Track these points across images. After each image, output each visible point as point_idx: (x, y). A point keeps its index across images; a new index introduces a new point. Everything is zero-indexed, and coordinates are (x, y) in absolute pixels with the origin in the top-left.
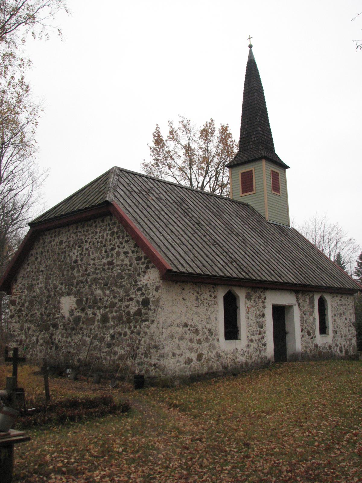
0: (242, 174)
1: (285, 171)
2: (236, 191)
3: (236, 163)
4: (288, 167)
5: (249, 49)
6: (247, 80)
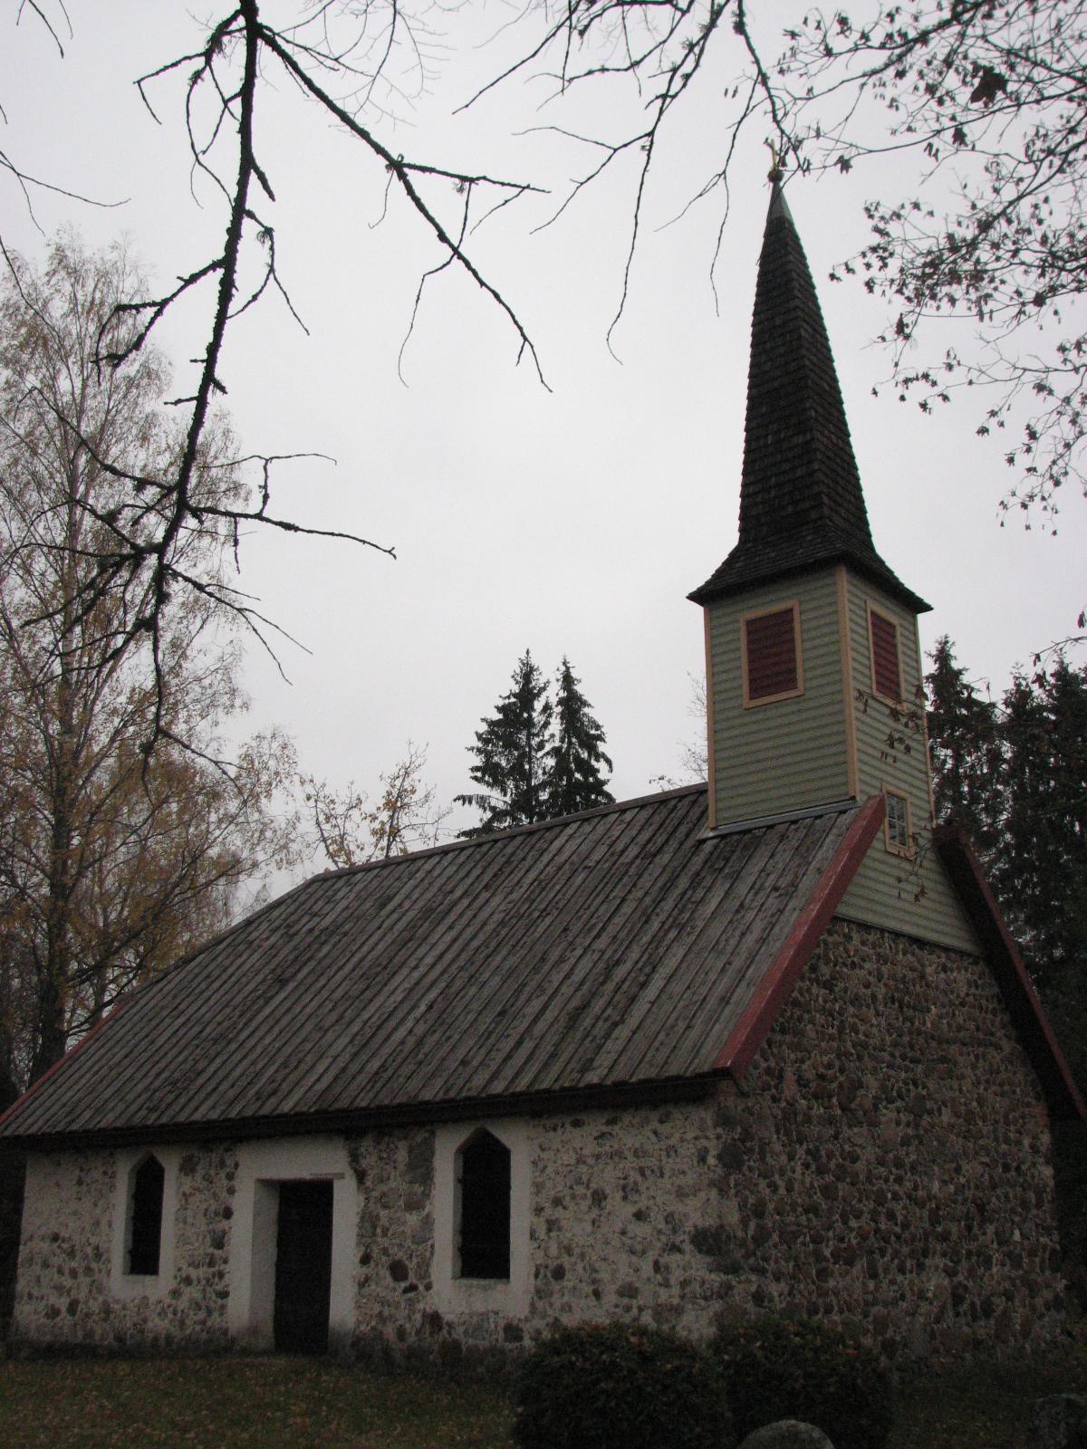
0: (750, 623)
1: (915, 619)
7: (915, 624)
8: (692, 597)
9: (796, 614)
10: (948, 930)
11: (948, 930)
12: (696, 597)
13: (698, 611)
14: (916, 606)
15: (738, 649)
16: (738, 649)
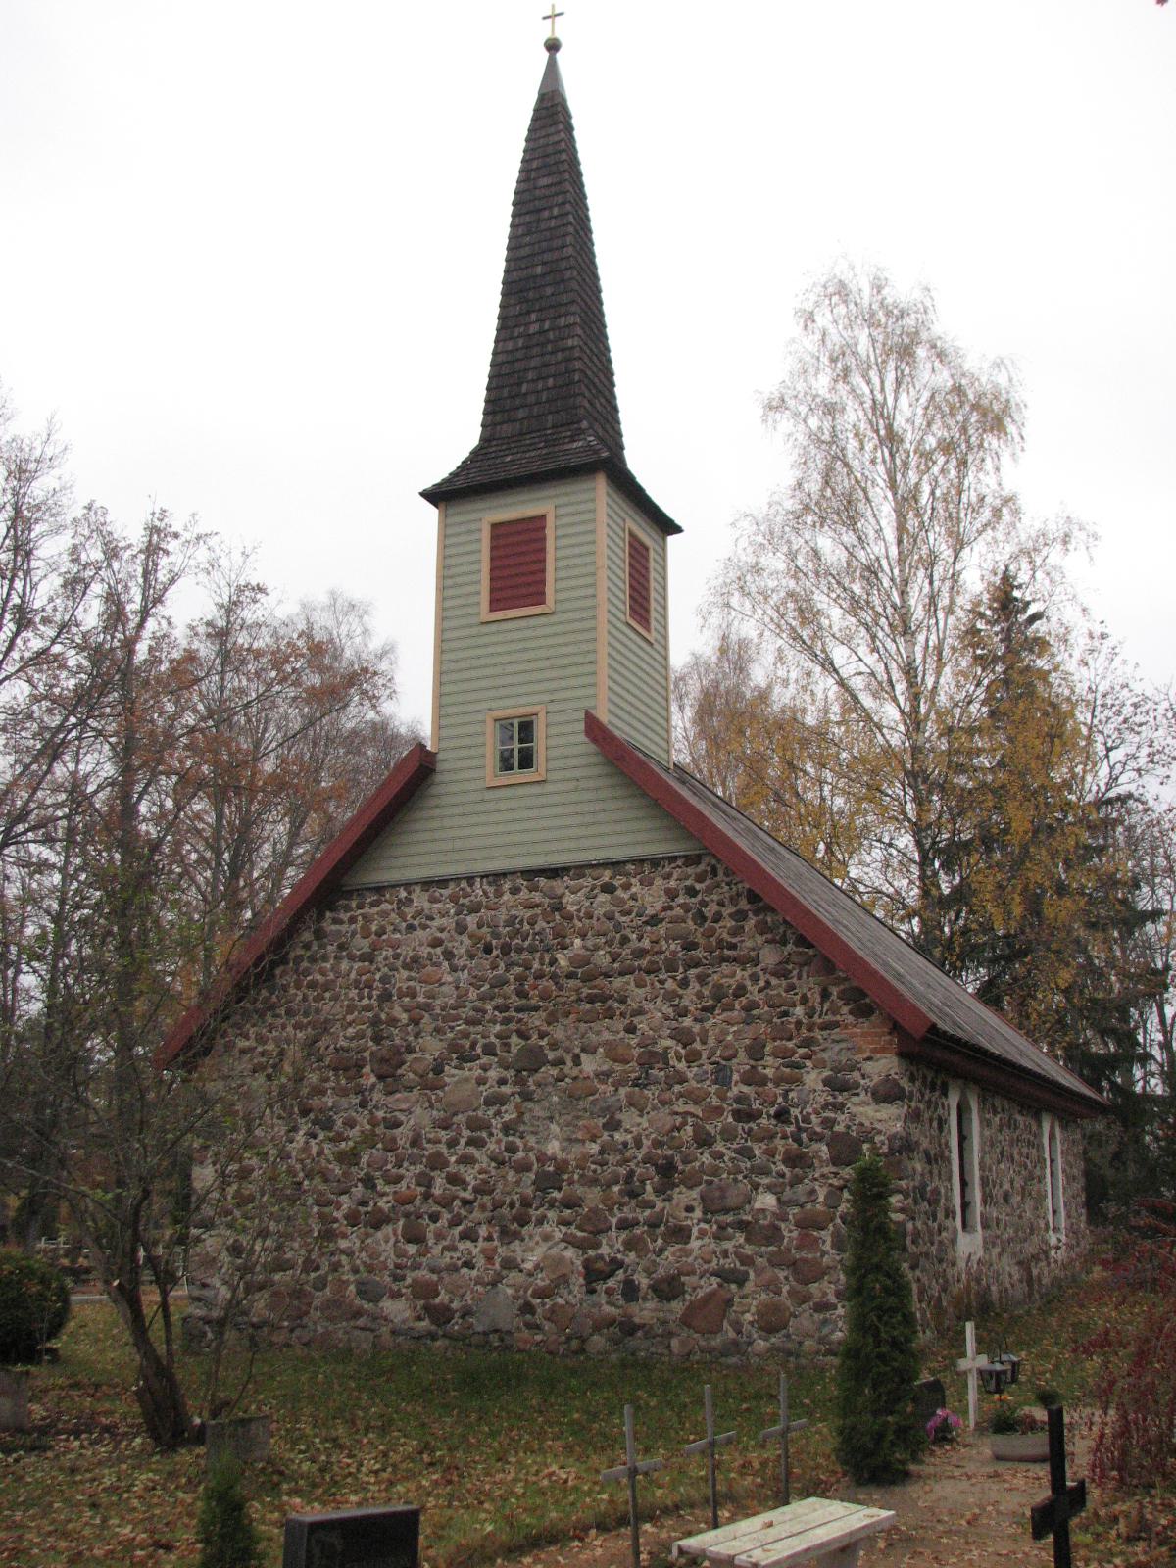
0: (495, 526)
1: (664, 540)
2: (466, 579)
3: (477, 478)
4: (678, 530)
5: (546, 55)
6: (499, 388)
7: (664, 548)
8: (422, 494)
9: (550, 523)
10: (640, 837)
11: (640, 837)
12: (436, 496)
13: (431, 513)
14: (667, 527)
15: (484, 744)
16: (478, 593)
